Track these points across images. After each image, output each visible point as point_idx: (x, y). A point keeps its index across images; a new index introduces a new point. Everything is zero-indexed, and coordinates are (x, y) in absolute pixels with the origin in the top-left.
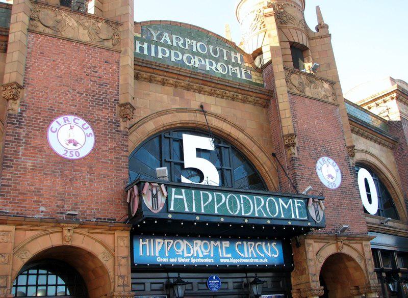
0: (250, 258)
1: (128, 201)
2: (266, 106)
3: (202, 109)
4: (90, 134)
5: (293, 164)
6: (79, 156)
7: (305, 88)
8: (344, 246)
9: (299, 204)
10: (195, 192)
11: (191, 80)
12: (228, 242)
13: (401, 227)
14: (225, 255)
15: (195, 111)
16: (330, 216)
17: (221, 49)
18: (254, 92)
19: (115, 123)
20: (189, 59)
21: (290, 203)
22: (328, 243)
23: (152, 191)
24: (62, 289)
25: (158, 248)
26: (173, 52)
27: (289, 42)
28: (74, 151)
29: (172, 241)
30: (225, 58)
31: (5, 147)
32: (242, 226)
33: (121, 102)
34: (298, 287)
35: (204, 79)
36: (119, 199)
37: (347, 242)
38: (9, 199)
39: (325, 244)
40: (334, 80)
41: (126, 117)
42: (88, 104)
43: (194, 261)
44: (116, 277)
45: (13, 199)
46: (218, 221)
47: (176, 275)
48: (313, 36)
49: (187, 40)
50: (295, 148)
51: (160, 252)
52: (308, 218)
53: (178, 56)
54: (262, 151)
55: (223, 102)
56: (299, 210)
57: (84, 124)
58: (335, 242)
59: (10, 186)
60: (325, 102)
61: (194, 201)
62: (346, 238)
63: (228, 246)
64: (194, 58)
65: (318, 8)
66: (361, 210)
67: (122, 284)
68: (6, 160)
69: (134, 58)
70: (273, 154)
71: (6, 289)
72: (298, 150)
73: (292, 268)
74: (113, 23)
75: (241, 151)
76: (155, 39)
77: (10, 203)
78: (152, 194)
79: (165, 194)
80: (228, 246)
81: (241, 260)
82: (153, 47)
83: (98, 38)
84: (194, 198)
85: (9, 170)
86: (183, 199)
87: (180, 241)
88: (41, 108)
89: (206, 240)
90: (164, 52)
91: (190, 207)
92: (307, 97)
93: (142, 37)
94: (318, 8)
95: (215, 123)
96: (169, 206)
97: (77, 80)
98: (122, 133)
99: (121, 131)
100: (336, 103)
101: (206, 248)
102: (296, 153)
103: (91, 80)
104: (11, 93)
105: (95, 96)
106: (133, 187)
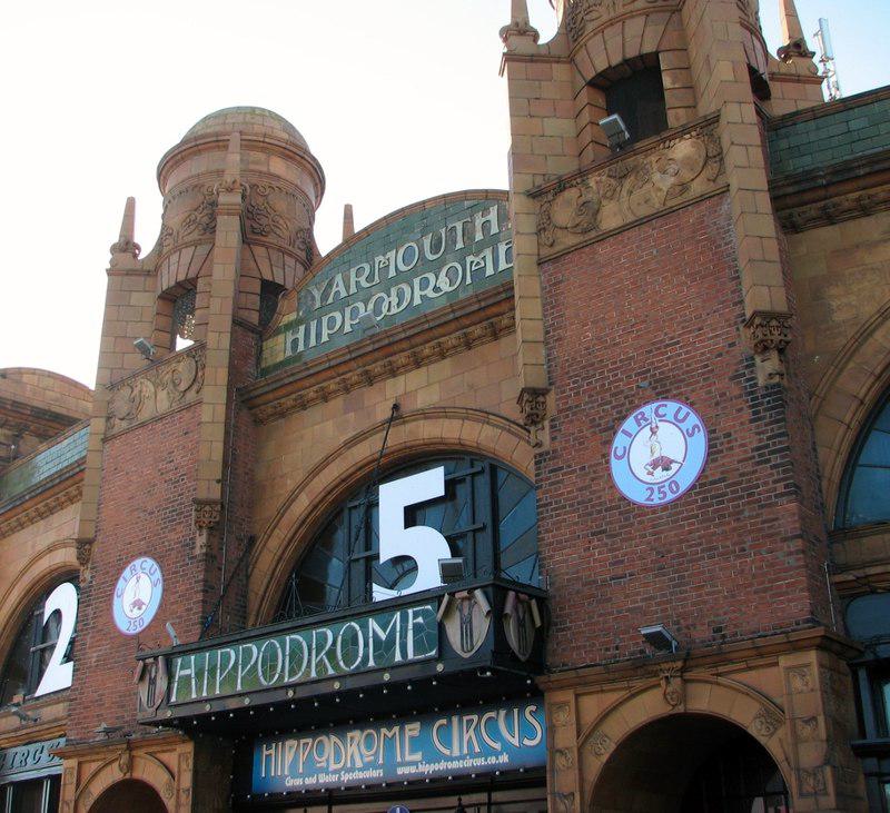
0: (462, 758)
3: (397, 415)
4: (696, 426)
6: (678, 489)
11: (360, 361)
14: (408, 758)
16: (642, 600)
18: (499, 302)
28: (667, 484)
29: (475, 717)
35: (376, 346)
43: (346, 778)
51: (290, 767)
52: (440, 651)
55: (443, 368)
57: (679, 410)
63: (416, 733)
80: (416, 733)
81: (441, 766)
87: (324, 738)
89: (370, 727)
101: (369, 746)
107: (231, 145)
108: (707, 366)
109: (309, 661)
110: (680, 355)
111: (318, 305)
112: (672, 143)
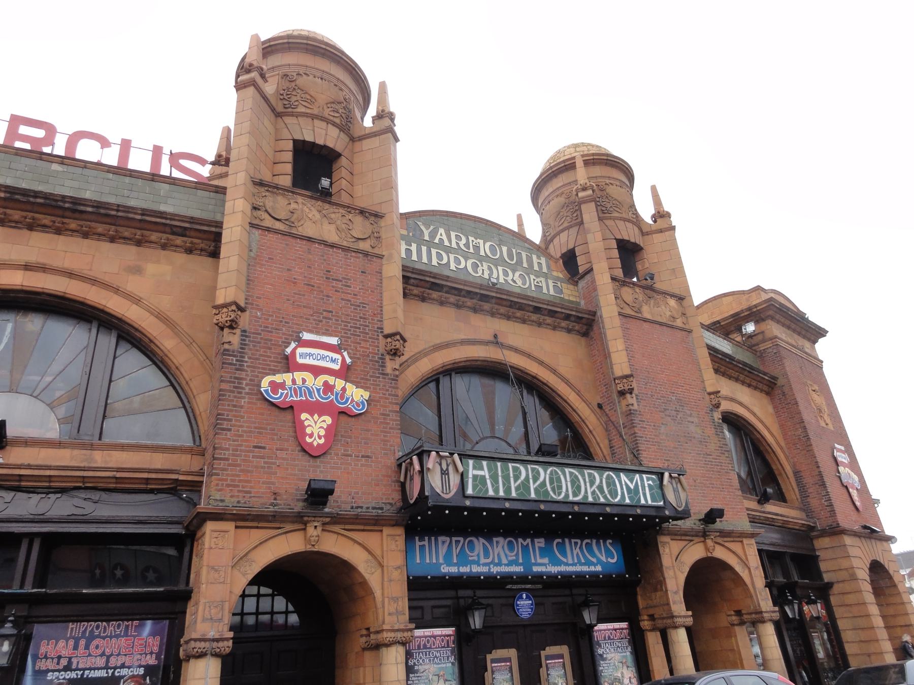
0: (573, 564)
1: (402, 479)
2: (585, 334)
3: (496, 341)
5: (632, 420)
7: (641, 307)
8: (717, 546)
9: (650, 482)
10: (501, 465)
12: (542, 540)
13: (799, 516)
14: (539, 561)
15: (487, 343)
17: (518, 251)
19: (378, 362)
20: (475, 266)
21: (637, 480)
22: (691, 541)
23: (440, 464)
24: (294, 619)
25: (443, 550)
26: (452, 256)
27: (615, 239)
29: (461, 539)
30: (525, 265)
31: (219, 400)
32: (537, 515)
33: (387, 331)
34: (651, 612)
36: (387, 476)
37: (719, 540)
38: (226, 480)
39: (687, 542)
40: (683, 294)
41: (395, 353)
43: (495, 570)
44: (386, 600)
45: (232, 480)
46: (537, 509)
47: (469, 593)
48: (649, 230)
49: (471, 239)
50: (634, 395)
52: (664, 502)
53: (460, 263)
54: (583, 400)
56: (650, 491)
58: (702, 539)
59: (227, 459)
60: (672, 327)
61: (500, 479)
62: (718, 534)
63: (543, 545)
64: (482, 266)
65: (654, 189)
66: (736, 489)
67: (394, 611)
68: (221, 419)
69: (403, 266)
70: (599, 404)
71: (222, 624)
72: (637, 399)
73: (639, 582)
74: (371, 214)
75: (552, 400)
76: (427, 238)
77: (228, 486)
78: (442, 469)
79: (461, 469)
81: (563, 568)
82: (424, 249)
83: (351, 237)
84: (500, 474)
85: (226, 434)
86: (484, 476)
88: (271, 340)
90: (439, 257)
91: (496, 490)
92: (646, 320)
93: (408, 233)
94: (654, 189)
96: (465, 487)
98: (389, 376)
99: (387, 375)
100: (687, 327)
102: (635, 404)
103: (342, 299)
104: (229, 318)
105: (349, 323)
106: (411, 459)
107: (578, 165)
109: (586, 489)
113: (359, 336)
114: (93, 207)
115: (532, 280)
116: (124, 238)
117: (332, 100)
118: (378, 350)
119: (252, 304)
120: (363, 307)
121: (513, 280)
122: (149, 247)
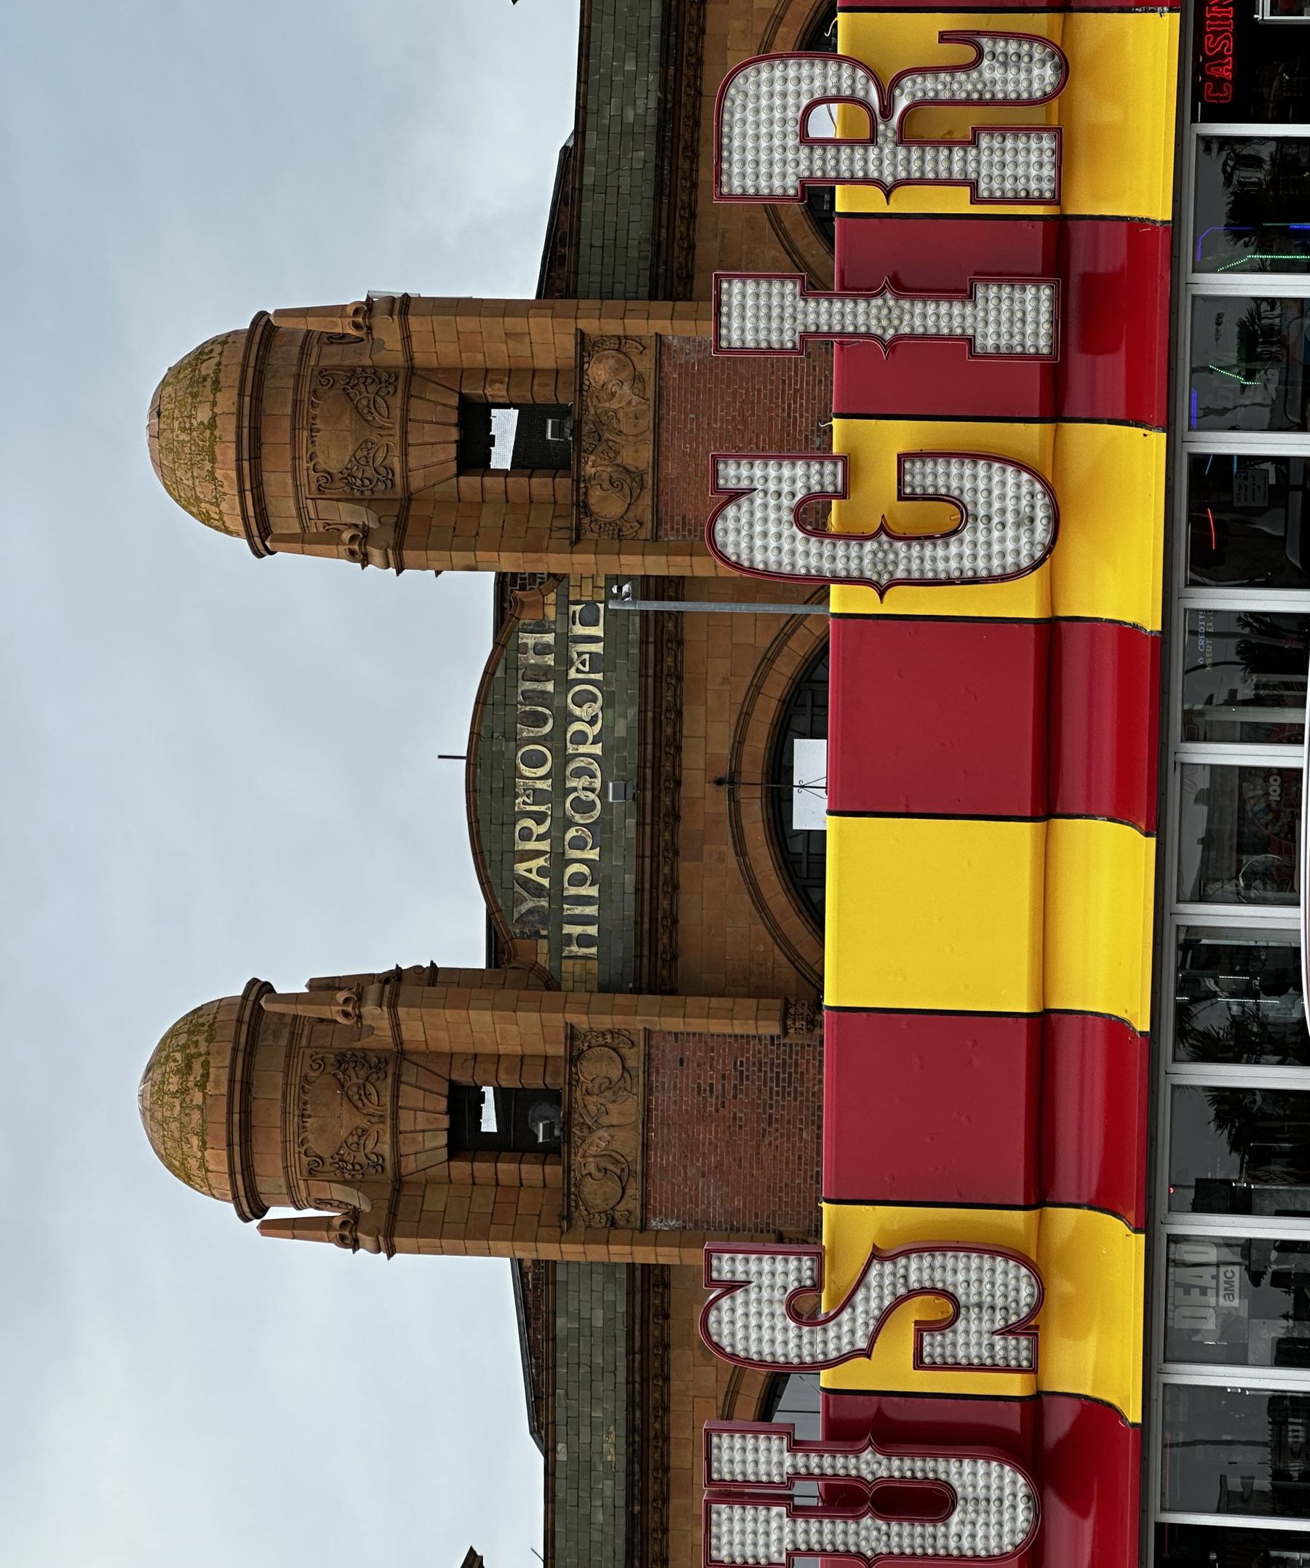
3: (730, 781)
30: (550, 687)
42: (793, 1103)
64: (575, 789)
76: (544, 903)
82: (569, 909)
95: (758, 744)
97: (740, 1127)
103: (735, 1097)
108: (820, 381)
110: (801, 404)
111: (544, 903)
112: (587, 383)
113: (790, 1074)
114: (634, 1411)
115: (580, 676)
116: (662, 1366)
117: (345, 1098)
118: (809, 1046)
119: (768, 1224)
120: (741, 1066)
121: (592, 722)
122: (669, 1334)
